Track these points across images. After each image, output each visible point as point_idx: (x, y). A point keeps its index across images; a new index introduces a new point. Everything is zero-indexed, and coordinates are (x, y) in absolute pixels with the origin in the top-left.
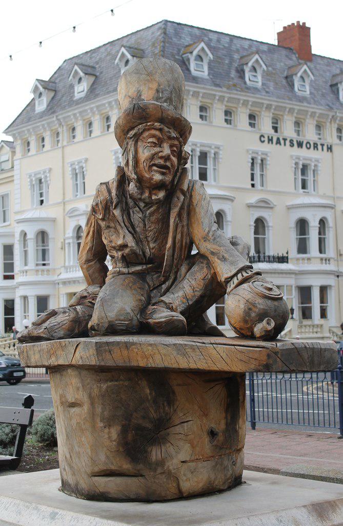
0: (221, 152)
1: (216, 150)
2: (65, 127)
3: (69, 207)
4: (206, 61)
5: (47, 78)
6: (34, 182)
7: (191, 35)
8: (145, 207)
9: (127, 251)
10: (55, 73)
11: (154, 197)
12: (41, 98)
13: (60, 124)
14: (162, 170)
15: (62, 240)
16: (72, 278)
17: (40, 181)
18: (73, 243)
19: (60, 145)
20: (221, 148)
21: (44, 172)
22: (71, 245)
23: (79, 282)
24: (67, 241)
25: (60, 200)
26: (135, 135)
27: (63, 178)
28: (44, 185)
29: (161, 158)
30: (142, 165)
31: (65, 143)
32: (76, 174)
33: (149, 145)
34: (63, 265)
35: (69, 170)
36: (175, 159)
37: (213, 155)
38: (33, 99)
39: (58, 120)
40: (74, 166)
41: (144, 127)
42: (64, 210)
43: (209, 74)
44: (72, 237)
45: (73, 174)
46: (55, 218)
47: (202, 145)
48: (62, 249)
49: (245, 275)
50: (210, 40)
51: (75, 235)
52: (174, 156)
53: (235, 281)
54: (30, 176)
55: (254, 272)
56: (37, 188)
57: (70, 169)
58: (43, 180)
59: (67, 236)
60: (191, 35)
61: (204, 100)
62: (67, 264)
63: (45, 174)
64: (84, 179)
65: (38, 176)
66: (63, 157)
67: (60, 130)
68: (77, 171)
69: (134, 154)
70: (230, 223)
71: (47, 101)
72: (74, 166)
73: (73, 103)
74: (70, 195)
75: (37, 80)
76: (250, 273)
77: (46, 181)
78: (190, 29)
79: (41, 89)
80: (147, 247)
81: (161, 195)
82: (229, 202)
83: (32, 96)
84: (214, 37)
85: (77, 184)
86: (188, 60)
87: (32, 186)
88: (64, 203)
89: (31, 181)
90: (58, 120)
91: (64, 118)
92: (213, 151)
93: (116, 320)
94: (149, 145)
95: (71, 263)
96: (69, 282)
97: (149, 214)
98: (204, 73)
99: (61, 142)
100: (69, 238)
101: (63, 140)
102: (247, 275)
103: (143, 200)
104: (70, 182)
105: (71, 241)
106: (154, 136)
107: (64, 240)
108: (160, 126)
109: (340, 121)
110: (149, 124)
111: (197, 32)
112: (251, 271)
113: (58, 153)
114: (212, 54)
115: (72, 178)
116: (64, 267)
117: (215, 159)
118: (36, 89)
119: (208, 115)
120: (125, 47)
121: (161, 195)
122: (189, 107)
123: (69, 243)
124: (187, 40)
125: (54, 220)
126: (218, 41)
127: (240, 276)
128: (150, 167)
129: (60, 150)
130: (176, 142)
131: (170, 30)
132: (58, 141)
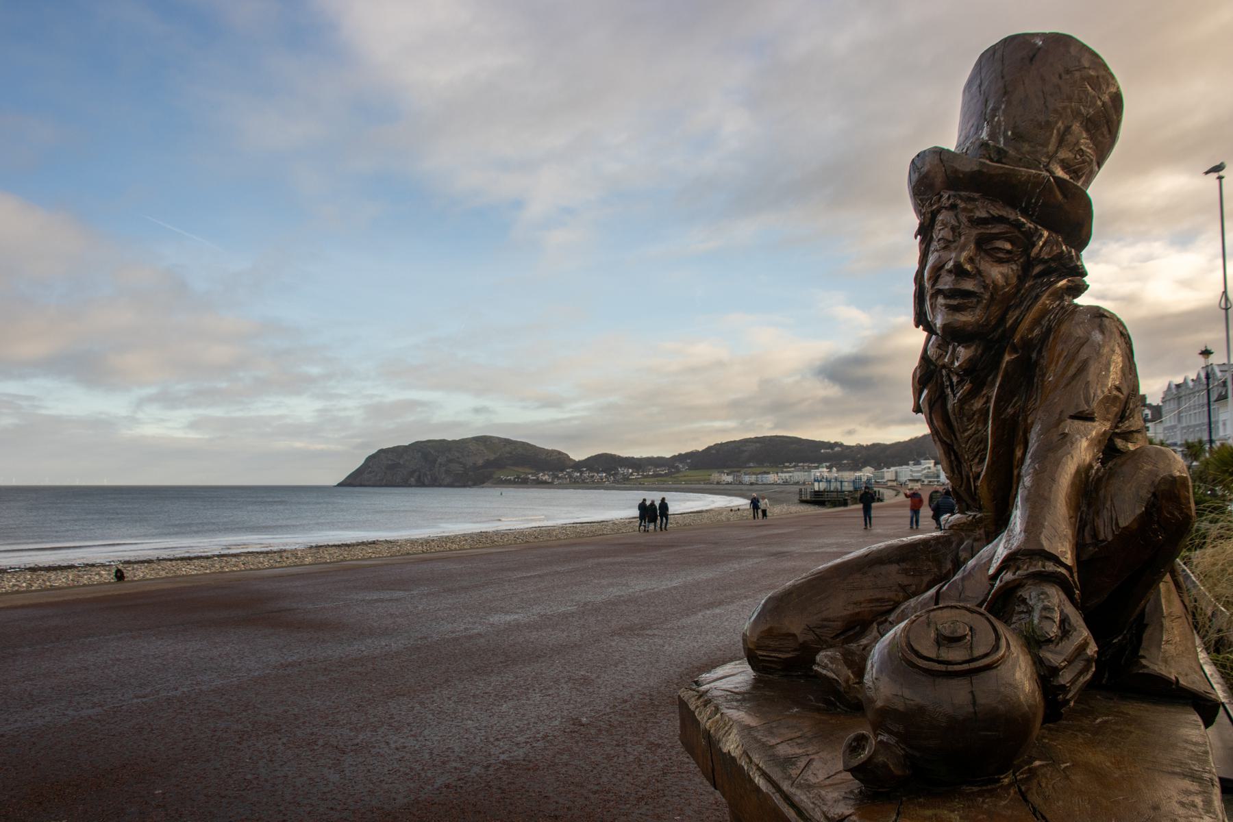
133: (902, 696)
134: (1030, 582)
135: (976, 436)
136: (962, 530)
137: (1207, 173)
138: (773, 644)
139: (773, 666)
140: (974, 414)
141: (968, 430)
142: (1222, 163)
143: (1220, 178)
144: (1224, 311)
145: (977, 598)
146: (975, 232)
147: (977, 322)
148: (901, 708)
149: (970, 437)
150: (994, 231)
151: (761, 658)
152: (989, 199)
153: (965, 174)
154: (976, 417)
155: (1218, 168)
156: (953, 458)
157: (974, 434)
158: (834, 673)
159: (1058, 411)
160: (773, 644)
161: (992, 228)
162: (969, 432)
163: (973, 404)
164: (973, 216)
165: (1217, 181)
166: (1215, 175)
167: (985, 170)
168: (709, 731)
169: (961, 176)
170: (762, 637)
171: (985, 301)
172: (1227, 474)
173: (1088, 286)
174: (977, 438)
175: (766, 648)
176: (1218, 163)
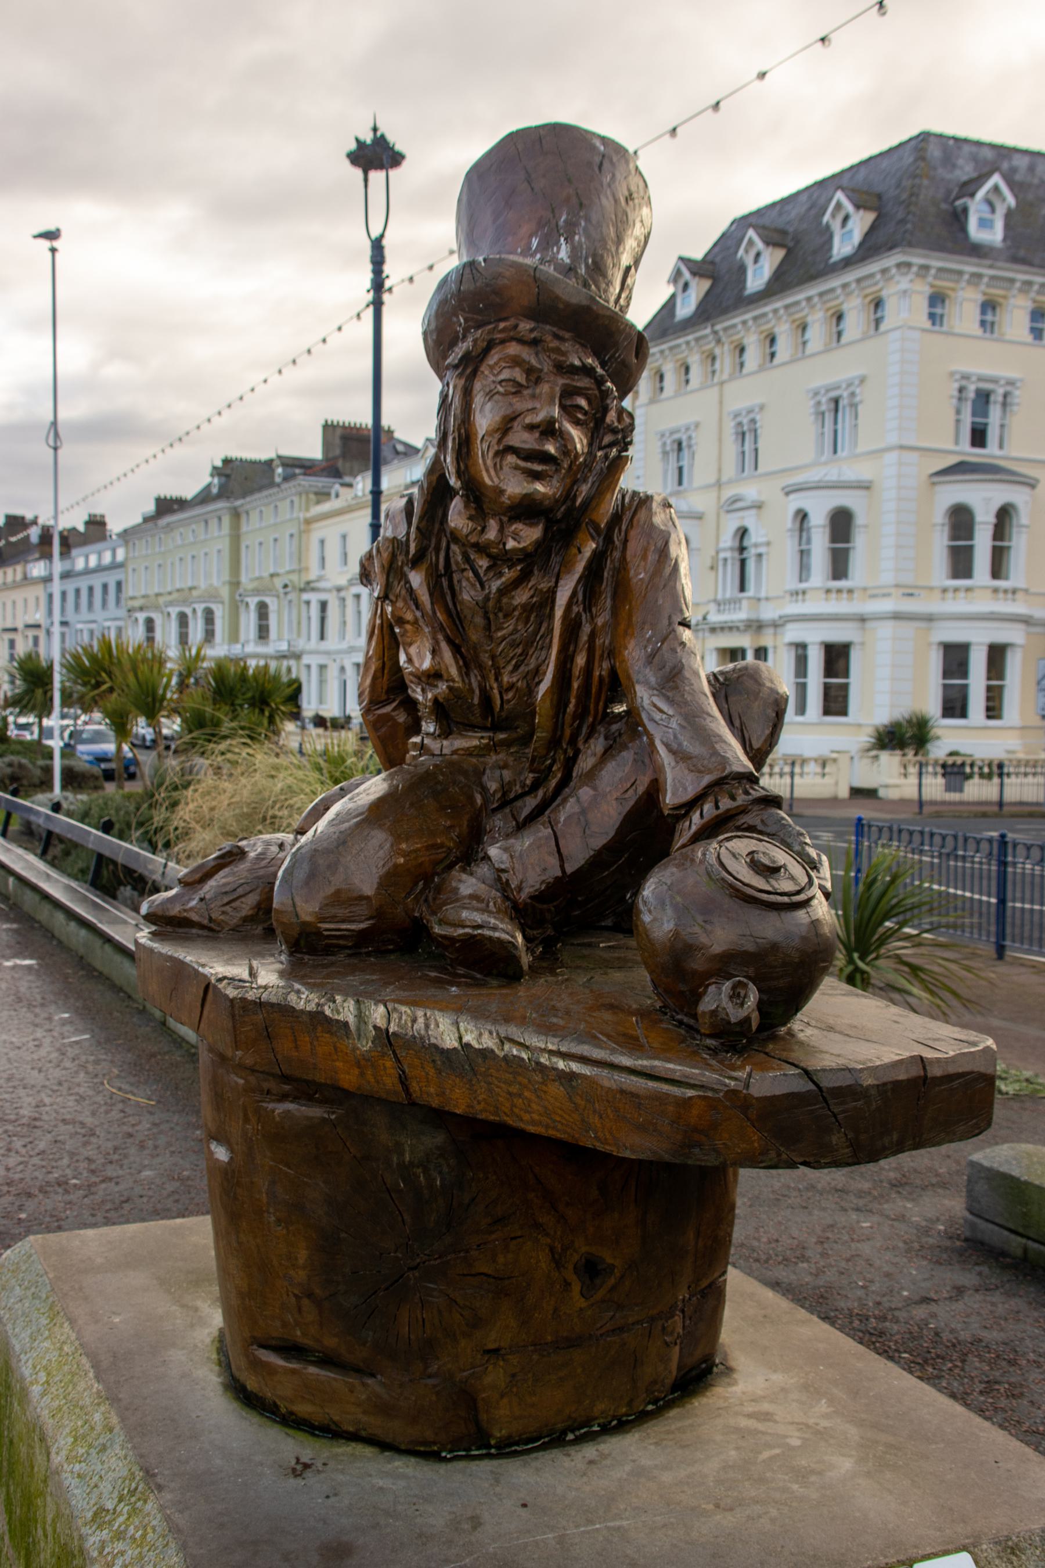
0: (1017, 393)
1: (1009, 388)
2: (726, 347)
3: (728, 493)
4: (1001, 211)
5: (698, 254)
6: (668, 448)
7: (974, 158)
8: (489, 569)
9: (443, 687)
10: (715, 245)
11: (511, 544)
12: (687, 293)
13: (719, 341)
14: (529, 465)
15: (713, 553)
16: (726, 622)
17: (680, 444)
18: (733, 558)
19: (716, 380)
20: (1018, 384)
21: (687, 429)
22: (729, 562)
23: (738, 628)
24: (722, 555)
25: (712, 479)
26: (466, 358)
27: (720, 440)
28: (686, 452)
29: (531, 427)
30: (483, 451)
31: (725, 376)
32: (743, 434)
33: (501, 389)
34: (712, 597)
35: (730, 427)
36: (578, 438)
37: (1000, 399)
38: (673, 297)
39: (715, 333)
40: (739, 419)
41: (489, 333)
42: (719, 498)
43: (1005, 239)
44: (732, 549)
45: (737, 434)
46: (871, 482)
47: (981, 379)
48: (712, 568)
49: (725, 804)
50: (1014, 170)
51: (737, 544)
52: (577, 423)
53: (696, 820)
54: (663, 435)
55: (759, 793)
56: (673, 457)
57: (733, 424)
58: (684, 444)
59: (722, 545)
60: (974, 158)
61: (938, 283)
62: (720, 597)
63: (689, 433)
64: (756, 442)
65: (676, 436)
66: (721, 402)
67: (717, 351)
68: (745, 428)
69: (458, 421)
70: (1024, 530)
71: (697, 296)
72: (739, 419)
73: (746, 301)
74: (730, 469)
75: (681, 259)
76: (741, 799)
77: (690, 446)
78: (974, 149)
79: (687, 275)
80: (495, 685)
81: (529, 535)
82: (1026, 490)
83: (670, 290)
84: (1022, 162)
85: (743, 453)
86: (965, 210)
87: (665, 453)
88: (719, 484)
89: (664, 444)
90: (715, 333)
91: (725, 329)
92: (1001, 391)
93: (323, 920)
94: (501, 389)
95: (728, 595)
96: (722, 629)
97: (499, 590)
98: (995, 235)
99: (717, 374)
100: (724, 550)
101: (722, 372)
102: (735, 804)
103: (482, 549)
104: (731, 448)
105: (728, 554)
106: (516, 362)
107: (717, 553)
108: (532, 330)
109: (1038, 293)
110: (502, 325)
111: (989, 154)
112: (747, 793)
113: (713, 393)
114: (1016, 196)
115: (736, 439)
116: (715, 601)
117: (1004, 405)
118: (676, 277)
119: (997, 319)
120: (843, 189)
121: (529, 535)
122: (961, 304)
123: (725, 560)
124: (966, 171)
125: (865, 486)
126: (1031, 169)
127: (708, 807)
128: (501, 453)
129: (716, 389)
130: (584, 382)
131: (934, 152)
132: (714, 372)
133: (751, 936)
134: (756, 808)
135: (514, 637)
136: (470, 755)
137: (35, 237)
138: (341, 912)
139: (342, 942)
140: (514, 610)
141: (503, 629)
142: (58, 230)
143: (53, 250)
144: (52, 451)
145: (607, 833)
146: (561, 381)
147: (554, 494)
148: (750, 947)
149: (504, 638)
150: (579, 384)
151: (326, 933)
152: (580, 343)
153: (568, 305)
154: (516, 613)
155: (51, 235)
156: (461, 663)
157: (511, 634)
158: (508, 933)
159: (666, 616)
160: (341, 912)
161: (578, 380)
162: (504, 632)
163: (513, 597)
164: (565, 361)
165: (49, 254)
166: (46, 244)
167: (595, 307)
168: (387, 1030)
169: (561, 306)
170: (327, 905)
171: (563, 471)
172: (89, 687)
173: (328, 428)
174: (514, 640)
175: (333, 919)
176: (52, 228)
